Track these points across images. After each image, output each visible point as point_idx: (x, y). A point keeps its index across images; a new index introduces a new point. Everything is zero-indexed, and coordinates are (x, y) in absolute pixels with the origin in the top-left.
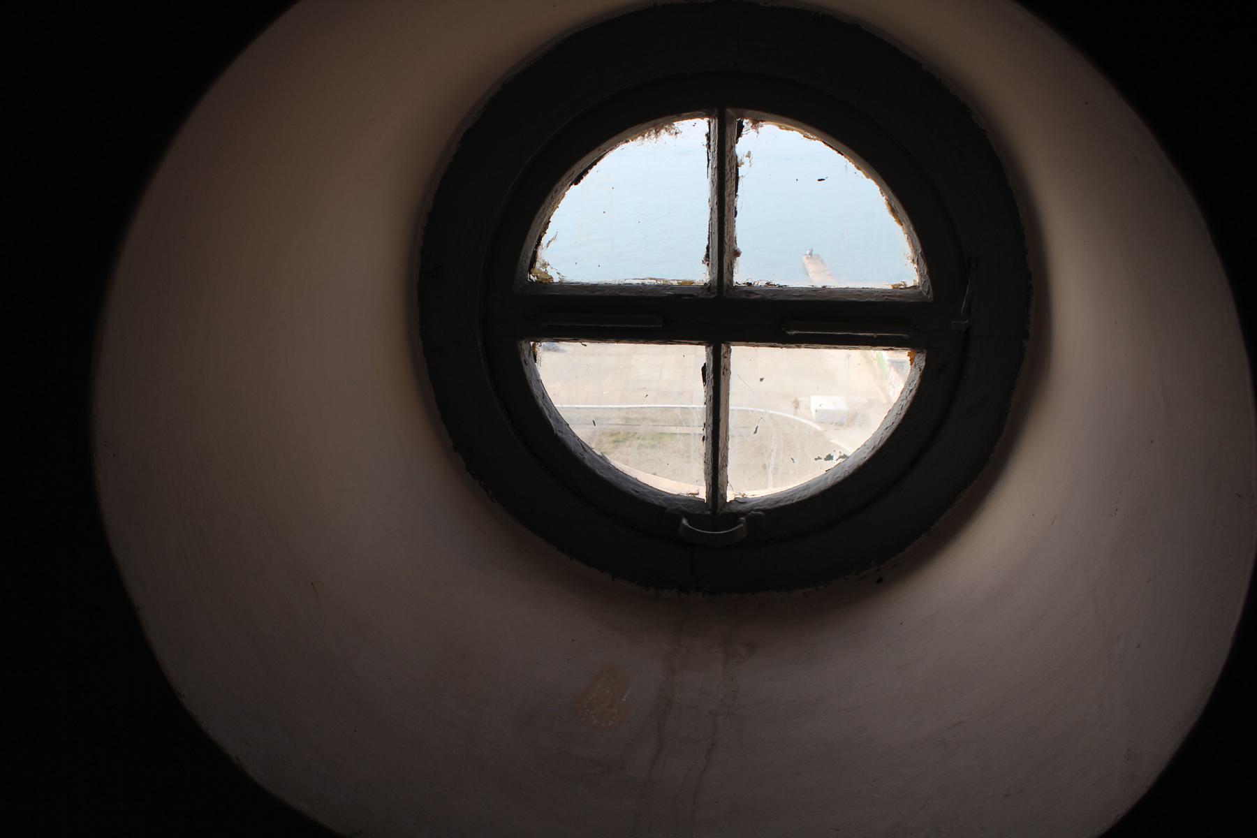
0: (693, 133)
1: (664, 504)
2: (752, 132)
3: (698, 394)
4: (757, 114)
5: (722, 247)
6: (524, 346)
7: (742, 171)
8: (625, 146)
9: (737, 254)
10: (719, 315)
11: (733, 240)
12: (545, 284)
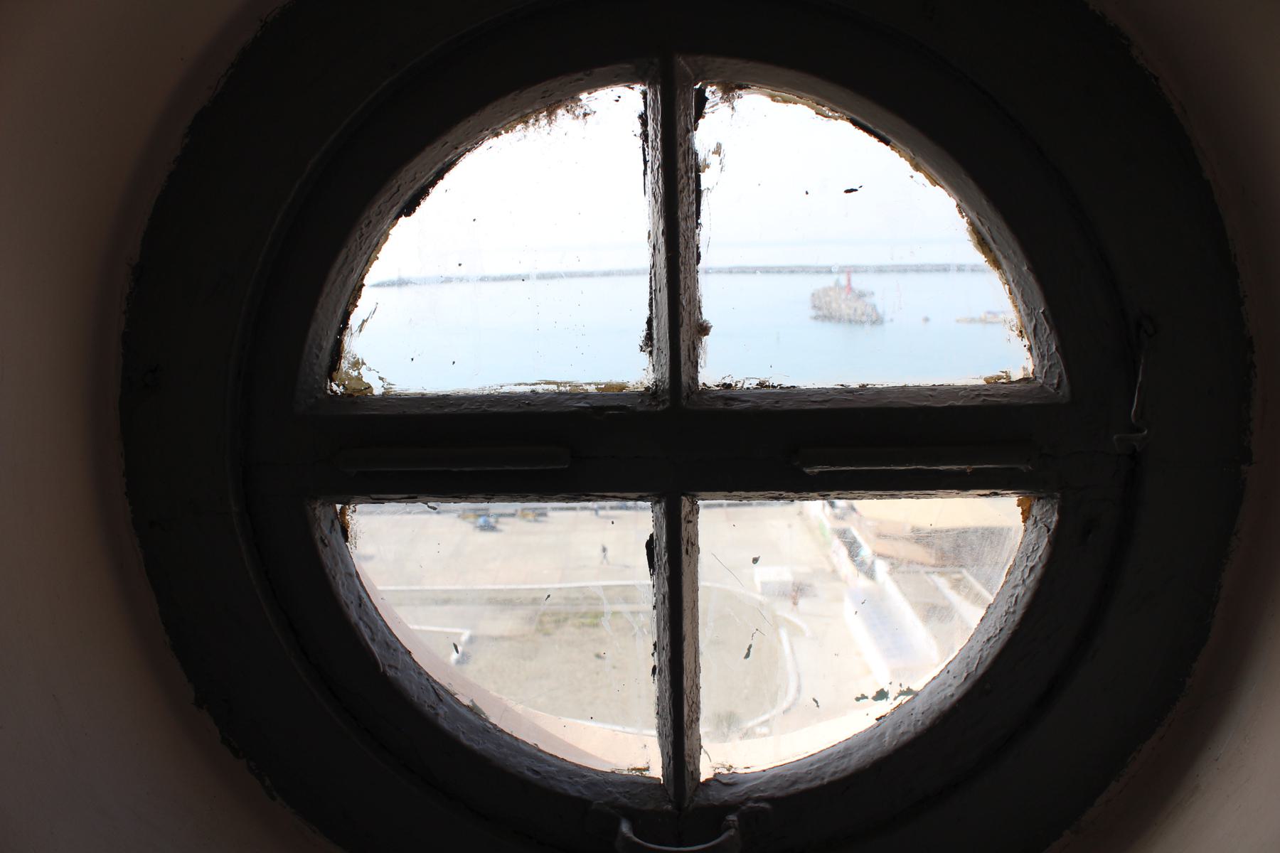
0: (614, 115)
1: (587, 794)
2: (724, 108)
3: (640, 581)
4: (734, 64)
5: (678, 319)
6: (321, 512)
7: (706, 179)
8: (492, 142)
9: (704, 329)
10: (677, 443)
11: (696, 304)
12: (359, 397)
